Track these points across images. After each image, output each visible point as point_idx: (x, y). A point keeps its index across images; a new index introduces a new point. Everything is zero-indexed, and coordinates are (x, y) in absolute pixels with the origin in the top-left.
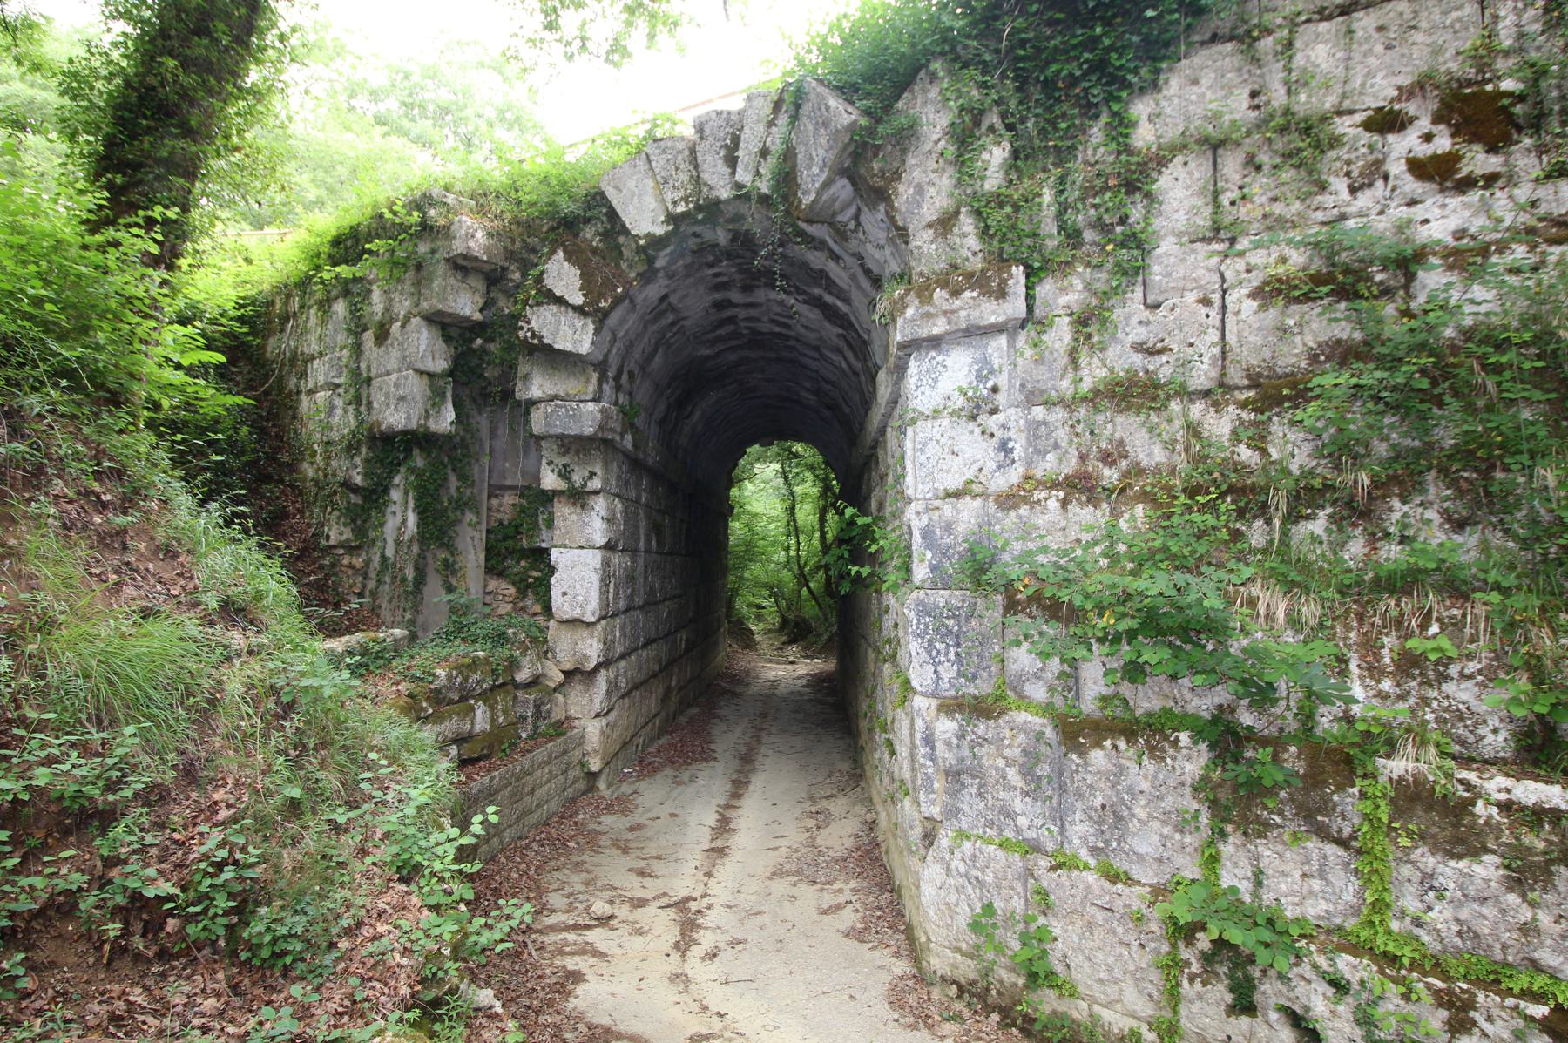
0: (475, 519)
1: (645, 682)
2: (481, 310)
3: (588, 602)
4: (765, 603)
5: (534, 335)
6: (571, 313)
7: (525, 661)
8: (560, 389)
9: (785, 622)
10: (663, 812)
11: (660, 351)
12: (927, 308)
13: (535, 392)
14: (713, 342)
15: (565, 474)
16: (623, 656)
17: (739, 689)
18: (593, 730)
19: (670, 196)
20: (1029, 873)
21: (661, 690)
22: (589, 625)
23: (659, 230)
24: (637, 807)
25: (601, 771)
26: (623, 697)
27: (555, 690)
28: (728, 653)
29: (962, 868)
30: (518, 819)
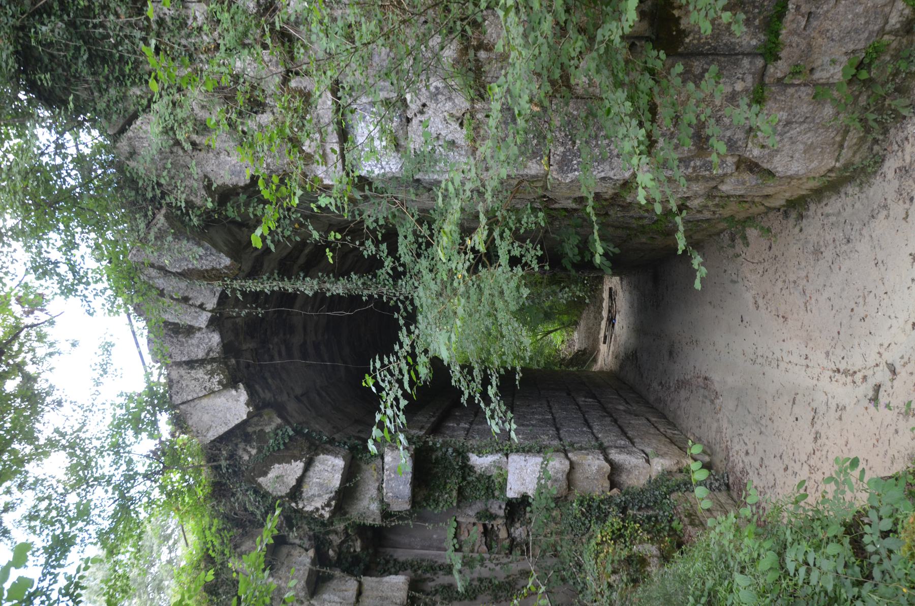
1: (620, 427)
2: (307, 550)
5: (328, 505)
6: (311, 473)
8: (373, 492)
12: (317, 157)
13: (374, 507)
18: (659, 465)
20: (780, 81)
23: (243, 396)
26: (633, 443)
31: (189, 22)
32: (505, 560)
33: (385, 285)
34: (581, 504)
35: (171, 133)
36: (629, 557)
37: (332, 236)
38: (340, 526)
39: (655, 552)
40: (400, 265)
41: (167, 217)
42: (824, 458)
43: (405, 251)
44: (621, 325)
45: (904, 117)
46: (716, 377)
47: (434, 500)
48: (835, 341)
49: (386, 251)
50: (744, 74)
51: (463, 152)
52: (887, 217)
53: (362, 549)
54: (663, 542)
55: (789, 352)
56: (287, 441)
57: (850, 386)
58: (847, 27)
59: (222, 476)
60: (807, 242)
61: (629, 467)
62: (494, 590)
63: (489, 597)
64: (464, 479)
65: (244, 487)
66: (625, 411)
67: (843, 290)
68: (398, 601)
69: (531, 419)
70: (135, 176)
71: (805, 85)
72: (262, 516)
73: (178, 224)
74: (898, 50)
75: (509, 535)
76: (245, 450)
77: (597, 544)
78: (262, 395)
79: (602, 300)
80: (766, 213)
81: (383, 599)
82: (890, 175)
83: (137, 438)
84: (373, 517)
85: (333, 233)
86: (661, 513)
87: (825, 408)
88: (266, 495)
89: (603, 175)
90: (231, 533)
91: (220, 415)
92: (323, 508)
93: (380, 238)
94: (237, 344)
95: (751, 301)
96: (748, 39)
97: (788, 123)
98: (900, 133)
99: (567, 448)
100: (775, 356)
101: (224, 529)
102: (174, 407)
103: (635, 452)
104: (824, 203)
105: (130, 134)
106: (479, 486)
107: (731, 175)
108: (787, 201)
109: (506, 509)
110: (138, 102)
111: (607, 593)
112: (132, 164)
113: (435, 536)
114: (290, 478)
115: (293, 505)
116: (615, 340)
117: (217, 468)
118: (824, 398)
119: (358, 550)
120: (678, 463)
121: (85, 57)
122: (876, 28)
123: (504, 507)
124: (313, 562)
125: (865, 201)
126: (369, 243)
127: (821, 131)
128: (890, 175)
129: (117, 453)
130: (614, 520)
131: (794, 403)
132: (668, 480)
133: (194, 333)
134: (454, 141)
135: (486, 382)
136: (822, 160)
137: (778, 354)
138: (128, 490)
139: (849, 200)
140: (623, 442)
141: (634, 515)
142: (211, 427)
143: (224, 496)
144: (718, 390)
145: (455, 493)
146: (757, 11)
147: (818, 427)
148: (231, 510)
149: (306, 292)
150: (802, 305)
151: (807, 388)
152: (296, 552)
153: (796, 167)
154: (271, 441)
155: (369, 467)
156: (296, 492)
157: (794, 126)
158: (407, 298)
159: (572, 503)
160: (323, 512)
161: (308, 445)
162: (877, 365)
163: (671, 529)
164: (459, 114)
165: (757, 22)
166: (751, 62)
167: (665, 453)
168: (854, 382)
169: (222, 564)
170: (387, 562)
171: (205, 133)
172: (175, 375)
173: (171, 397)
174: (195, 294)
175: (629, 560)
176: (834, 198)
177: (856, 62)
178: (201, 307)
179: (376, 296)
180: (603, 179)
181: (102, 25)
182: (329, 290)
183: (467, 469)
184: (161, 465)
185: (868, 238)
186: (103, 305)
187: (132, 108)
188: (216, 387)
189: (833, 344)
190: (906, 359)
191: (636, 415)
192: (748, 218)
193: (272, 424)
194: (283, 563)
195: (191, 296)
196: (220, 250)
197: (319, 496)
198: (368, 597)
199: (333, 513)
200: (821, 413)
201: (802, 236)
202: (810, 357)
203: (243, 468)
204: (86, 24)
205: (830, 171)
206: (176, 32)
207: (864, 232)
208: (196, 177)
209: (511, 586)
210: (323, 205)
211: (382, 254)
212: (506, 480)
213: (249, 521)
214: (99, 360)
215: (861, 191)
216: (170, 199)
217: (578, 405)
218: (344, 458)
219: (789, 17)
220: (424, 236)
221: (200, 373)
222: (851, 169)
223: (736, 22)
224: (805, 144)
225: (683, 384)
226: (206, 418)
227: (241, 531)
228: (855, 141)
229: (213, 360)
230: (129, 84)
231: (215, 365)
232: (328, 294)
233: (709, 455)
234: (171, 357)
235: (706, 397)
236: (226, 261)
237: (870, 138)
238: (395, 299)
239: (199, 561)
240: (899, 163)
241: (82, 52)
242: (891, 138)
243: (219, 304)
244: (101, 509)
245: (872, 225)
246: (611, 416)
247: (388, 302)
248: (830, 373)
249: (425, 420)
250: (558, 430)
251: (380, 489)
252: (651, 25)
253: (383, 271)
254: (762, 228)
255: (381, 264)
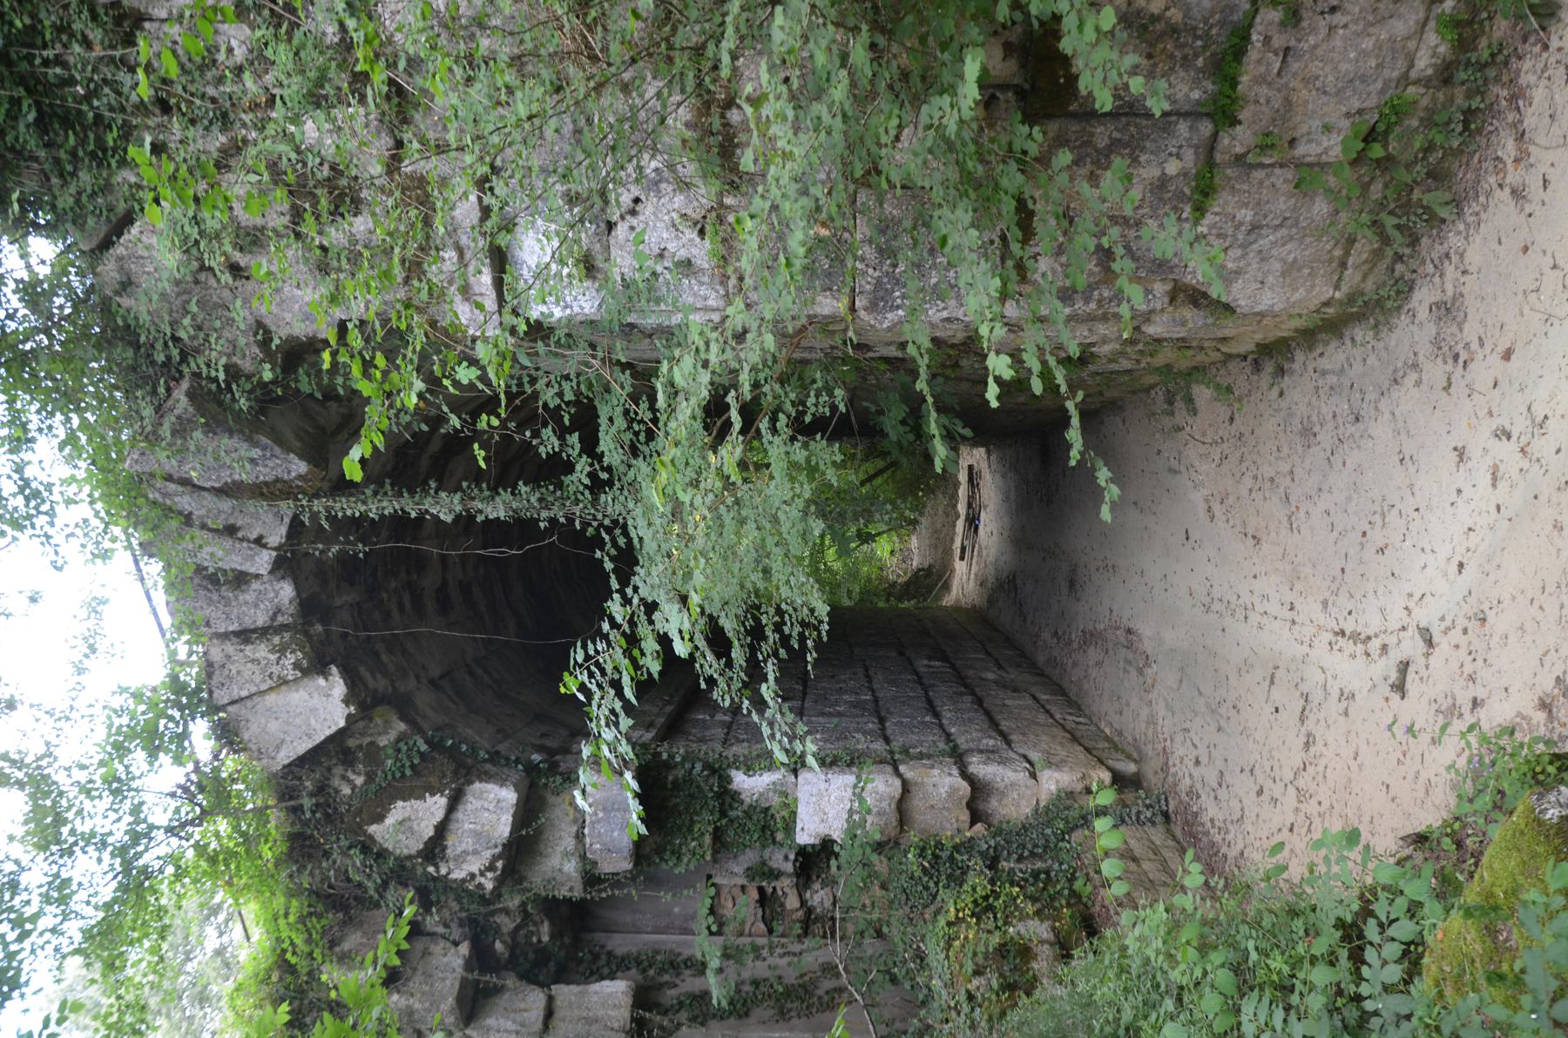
1: (988, 713)
2: (456, 944)
5: (491, 868)
8: (569, 843)
13: (571, 867)
18: (1052, 782)
20: (1239, 159)
21: (1001, 694)
22: (906, 787)
23: (338, 687)
26: (1008, 743)
29: (1235, 253)
31: (221, 57)
32: (797, 948)
33: (577, 502)
34: (922, 853)
35: (194, 251)
36: (1003, 945)
37: (483, 422)
38: (514, 902)
39: (1045, 936)
40: (603, 468)
41: (191, 395)
42: (1320, 778)
43: (612, 446)
44: (988, 529)
45: (1443, 221)
46: (1145, 629)
47: (673, 852)
48: (1337, 583)
49: (578, 446)
50: (1181, 147)
51: (706, 279)
52: (1418, 383)
53: (552, 937)
54: (1058, 918)
55: (1266, 597)
56: (416, 761)
57: (1361, 659)
58: (1347, 73)
59: (306, 823)
60: (1291, 415)
61: (1001, 786)
62: (778, 1000)
63: (771, 1012)
64: (723, 814)
65: (344, 843)
66: (995, 682)
67: (1349, 499)
68: (616, 1025)
69: (837, 703)
70: (133, 323)
71: (1282, 166)
72: (377, 890)
73: (212, 407)
74: (1432, 110)
75: (803, 903)
76: (344, 778)
77: (949, 924)
78: (371, 684)
79: (957, 484)
80: (1224, 363)
81: (590, 1021)
82: (1423, 313)
83: (151, 764)
84: (569, 884)
85: (484, 417)
86: (1056, 866)
87: (1320, 692)
88: (382, 854)
89: (945, 314)
90: (324, 922)
91: (298, 721)
92: (482, 874)
93: (567, 422)
94: (324, 597)
95: (1202, 506)
96: (1185, 89)
97: (1255, 228)
98: (1437, 246)
99: (897, 756)
100: (1241, 601)
101: (310, 914)
102: (214, 709)
103: (1011, 760)
104: (1319, 351)
105: (119, 250)
106: (749, 825)
107: (1162, 310)
108: (1258, 345)
109: (796, 860)
110: (133, 195)
111: (966, 1008)
112: (126, 302)
113: (676, 910)
114: (423, 824)
115: (431, 869)
116: (980, 555)
117: (296, 810)
118: (1320, 678)
119: (545, 938)
120: (1083, 777)
121: (31, 117)
122: (1396, 74)
123: (792, 857)
124: (468, 966)
125: (1383, 354)
126: (547, 433)
127: (1308, 240)
128: (1423, 313)
129: (115, 793)
130: (978, 881)
131: (1272, 682)
132: (1067, 808)
133: (247, 583)
134: (689, 262)
135: (755, 673)
136: (1312, 287)
137: (1246, 599)
138: (139, 855)
139: (1358, 352)
140: (991, 742)
141: (1012, 870)
142: (283, 741)
143: (310, 856)
144: (1149, 652)
145: (708, 839)
146: (1199, 43)
147: (1310, 724)
148: (322, 881)
149: (442, 517)
150: (1285, 523)
151: (1293, 659)
152: (437, 948)
153: (1269, 299)
154: (389, 762)
155: (559, 799)
156: (435, 848)
157: (1264, 232)
158: (615, 522)
159: (906, 852)
160: (483, 880)
161: (452, 767)
162: (1404, 628)
163: (1073, 893)
164: (697, 216)
165: (1200, 62)
166: (1191, 128)
167: (1063, 761)
168: (1368, 655)
169: (310, 973)
170: (596, 957)
171: (255, 249)
172: (216, 655)
173: (211, 693)
174: (248, 520)
175: (1002, 951)
176: (1334, 344)
177: (1364, 129)
178: (259, 542)
179: (562, 520)
180: (948, 320)
181: (59, 61)
182: (481, 512)
183: (727, 796)
184: (198, 809)
185: (1387, 416)
186: (83, 546)
187: (122, 206)
188: (291, 674)
189: (1334, 588)
190: (1448, 623)
191: (1015, 690)
192: (1196, 368)
193: (390, 731)
194: (415, 970)
195: (239, 523)
196: (288, 449)
197: (476, 852)
198: (563, 1020)
199: (500, 882)
200: (1316, 702)
201: (1284, 404)
202: (1298, 606)
203: (343, 809)
204: (30, 58)
205: (1327, 304)
206: (197, 74)
207: (1382, 405)
208: (242, 327)
209: (806, 991)
210: (465, 382)
211: (570, 451)
212: (794, 814)
213: (356, 899)
214: (81, 629)
215: (1377, 337)
216: (197, 363)
217: (917, 674)
218: (517, 790)
219: (1253, 54)
220: (641, 422)
221: (261, 651)
222: (1360, 303)
223: (1155, 93)
224: (1284, 261)
225: (1092, 637)
226: (273, 726)
227: (340, 915)
228: (1365, 256)
229: (284, 627)
230: (114, 164)
231: (287, 635)
232: (480, 518)
233: (1136, 761)
234: (208, 624)
235: (1129, 662)
236: (300, 467)
237: (1389, 253)
238: (595, 524)
239: (269, 971)
240: (1435, 296)
241: (25, 108)
242: (1424, 253)
243: (289, 536)
244: (92, 891)
245: (1395, 394)
246: (973, 693)
247: (584, 530)
248: (1330, 636)
249: (655, 710)
250: (882, 721)
251: (580, 837)
252: (1023, 66)
253: (574, 477)
254: (1218, 387)
255: (569, 468)
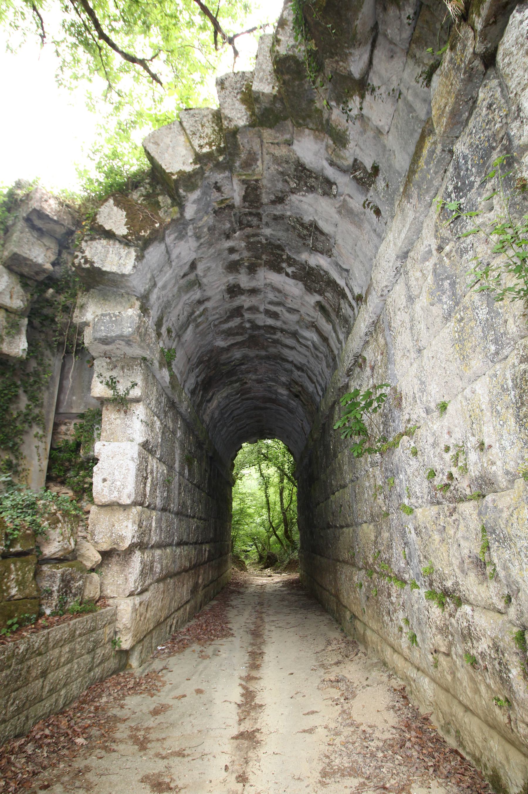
0: (41, 433)
1: (178, 573)
3: (124, 486)
4: (249, 549)
5: (86, 261)
6: (117, 245)
7: (55, 534)
9: (261, 558)
10: (189, 688)
11: (191, 327)
14: (229, 333)
15: (112, 384)
16: (159, 546)
17: (242, 590)
19: (196, 143)
21: (191, 583)
22: (125, 507)
23: (189, 169)
24: (164, 684)
25: (133, 648)
26: (158, 581)
27: (93, 570)
28: (232, 570)
30: (19, 711)
66: (197, 582)
113: (74, 398)
140: (158, 570)
217: (202, 543)
246: (190, 568)
